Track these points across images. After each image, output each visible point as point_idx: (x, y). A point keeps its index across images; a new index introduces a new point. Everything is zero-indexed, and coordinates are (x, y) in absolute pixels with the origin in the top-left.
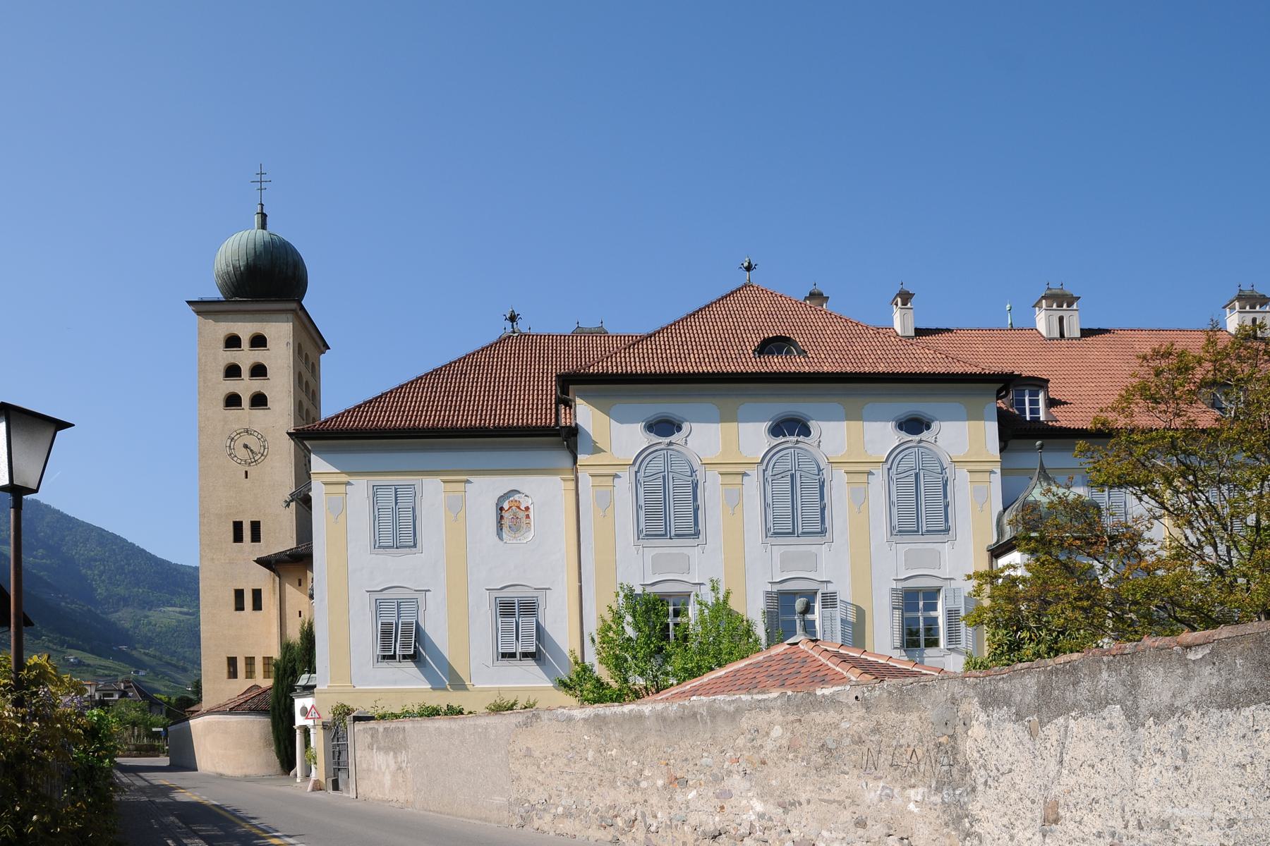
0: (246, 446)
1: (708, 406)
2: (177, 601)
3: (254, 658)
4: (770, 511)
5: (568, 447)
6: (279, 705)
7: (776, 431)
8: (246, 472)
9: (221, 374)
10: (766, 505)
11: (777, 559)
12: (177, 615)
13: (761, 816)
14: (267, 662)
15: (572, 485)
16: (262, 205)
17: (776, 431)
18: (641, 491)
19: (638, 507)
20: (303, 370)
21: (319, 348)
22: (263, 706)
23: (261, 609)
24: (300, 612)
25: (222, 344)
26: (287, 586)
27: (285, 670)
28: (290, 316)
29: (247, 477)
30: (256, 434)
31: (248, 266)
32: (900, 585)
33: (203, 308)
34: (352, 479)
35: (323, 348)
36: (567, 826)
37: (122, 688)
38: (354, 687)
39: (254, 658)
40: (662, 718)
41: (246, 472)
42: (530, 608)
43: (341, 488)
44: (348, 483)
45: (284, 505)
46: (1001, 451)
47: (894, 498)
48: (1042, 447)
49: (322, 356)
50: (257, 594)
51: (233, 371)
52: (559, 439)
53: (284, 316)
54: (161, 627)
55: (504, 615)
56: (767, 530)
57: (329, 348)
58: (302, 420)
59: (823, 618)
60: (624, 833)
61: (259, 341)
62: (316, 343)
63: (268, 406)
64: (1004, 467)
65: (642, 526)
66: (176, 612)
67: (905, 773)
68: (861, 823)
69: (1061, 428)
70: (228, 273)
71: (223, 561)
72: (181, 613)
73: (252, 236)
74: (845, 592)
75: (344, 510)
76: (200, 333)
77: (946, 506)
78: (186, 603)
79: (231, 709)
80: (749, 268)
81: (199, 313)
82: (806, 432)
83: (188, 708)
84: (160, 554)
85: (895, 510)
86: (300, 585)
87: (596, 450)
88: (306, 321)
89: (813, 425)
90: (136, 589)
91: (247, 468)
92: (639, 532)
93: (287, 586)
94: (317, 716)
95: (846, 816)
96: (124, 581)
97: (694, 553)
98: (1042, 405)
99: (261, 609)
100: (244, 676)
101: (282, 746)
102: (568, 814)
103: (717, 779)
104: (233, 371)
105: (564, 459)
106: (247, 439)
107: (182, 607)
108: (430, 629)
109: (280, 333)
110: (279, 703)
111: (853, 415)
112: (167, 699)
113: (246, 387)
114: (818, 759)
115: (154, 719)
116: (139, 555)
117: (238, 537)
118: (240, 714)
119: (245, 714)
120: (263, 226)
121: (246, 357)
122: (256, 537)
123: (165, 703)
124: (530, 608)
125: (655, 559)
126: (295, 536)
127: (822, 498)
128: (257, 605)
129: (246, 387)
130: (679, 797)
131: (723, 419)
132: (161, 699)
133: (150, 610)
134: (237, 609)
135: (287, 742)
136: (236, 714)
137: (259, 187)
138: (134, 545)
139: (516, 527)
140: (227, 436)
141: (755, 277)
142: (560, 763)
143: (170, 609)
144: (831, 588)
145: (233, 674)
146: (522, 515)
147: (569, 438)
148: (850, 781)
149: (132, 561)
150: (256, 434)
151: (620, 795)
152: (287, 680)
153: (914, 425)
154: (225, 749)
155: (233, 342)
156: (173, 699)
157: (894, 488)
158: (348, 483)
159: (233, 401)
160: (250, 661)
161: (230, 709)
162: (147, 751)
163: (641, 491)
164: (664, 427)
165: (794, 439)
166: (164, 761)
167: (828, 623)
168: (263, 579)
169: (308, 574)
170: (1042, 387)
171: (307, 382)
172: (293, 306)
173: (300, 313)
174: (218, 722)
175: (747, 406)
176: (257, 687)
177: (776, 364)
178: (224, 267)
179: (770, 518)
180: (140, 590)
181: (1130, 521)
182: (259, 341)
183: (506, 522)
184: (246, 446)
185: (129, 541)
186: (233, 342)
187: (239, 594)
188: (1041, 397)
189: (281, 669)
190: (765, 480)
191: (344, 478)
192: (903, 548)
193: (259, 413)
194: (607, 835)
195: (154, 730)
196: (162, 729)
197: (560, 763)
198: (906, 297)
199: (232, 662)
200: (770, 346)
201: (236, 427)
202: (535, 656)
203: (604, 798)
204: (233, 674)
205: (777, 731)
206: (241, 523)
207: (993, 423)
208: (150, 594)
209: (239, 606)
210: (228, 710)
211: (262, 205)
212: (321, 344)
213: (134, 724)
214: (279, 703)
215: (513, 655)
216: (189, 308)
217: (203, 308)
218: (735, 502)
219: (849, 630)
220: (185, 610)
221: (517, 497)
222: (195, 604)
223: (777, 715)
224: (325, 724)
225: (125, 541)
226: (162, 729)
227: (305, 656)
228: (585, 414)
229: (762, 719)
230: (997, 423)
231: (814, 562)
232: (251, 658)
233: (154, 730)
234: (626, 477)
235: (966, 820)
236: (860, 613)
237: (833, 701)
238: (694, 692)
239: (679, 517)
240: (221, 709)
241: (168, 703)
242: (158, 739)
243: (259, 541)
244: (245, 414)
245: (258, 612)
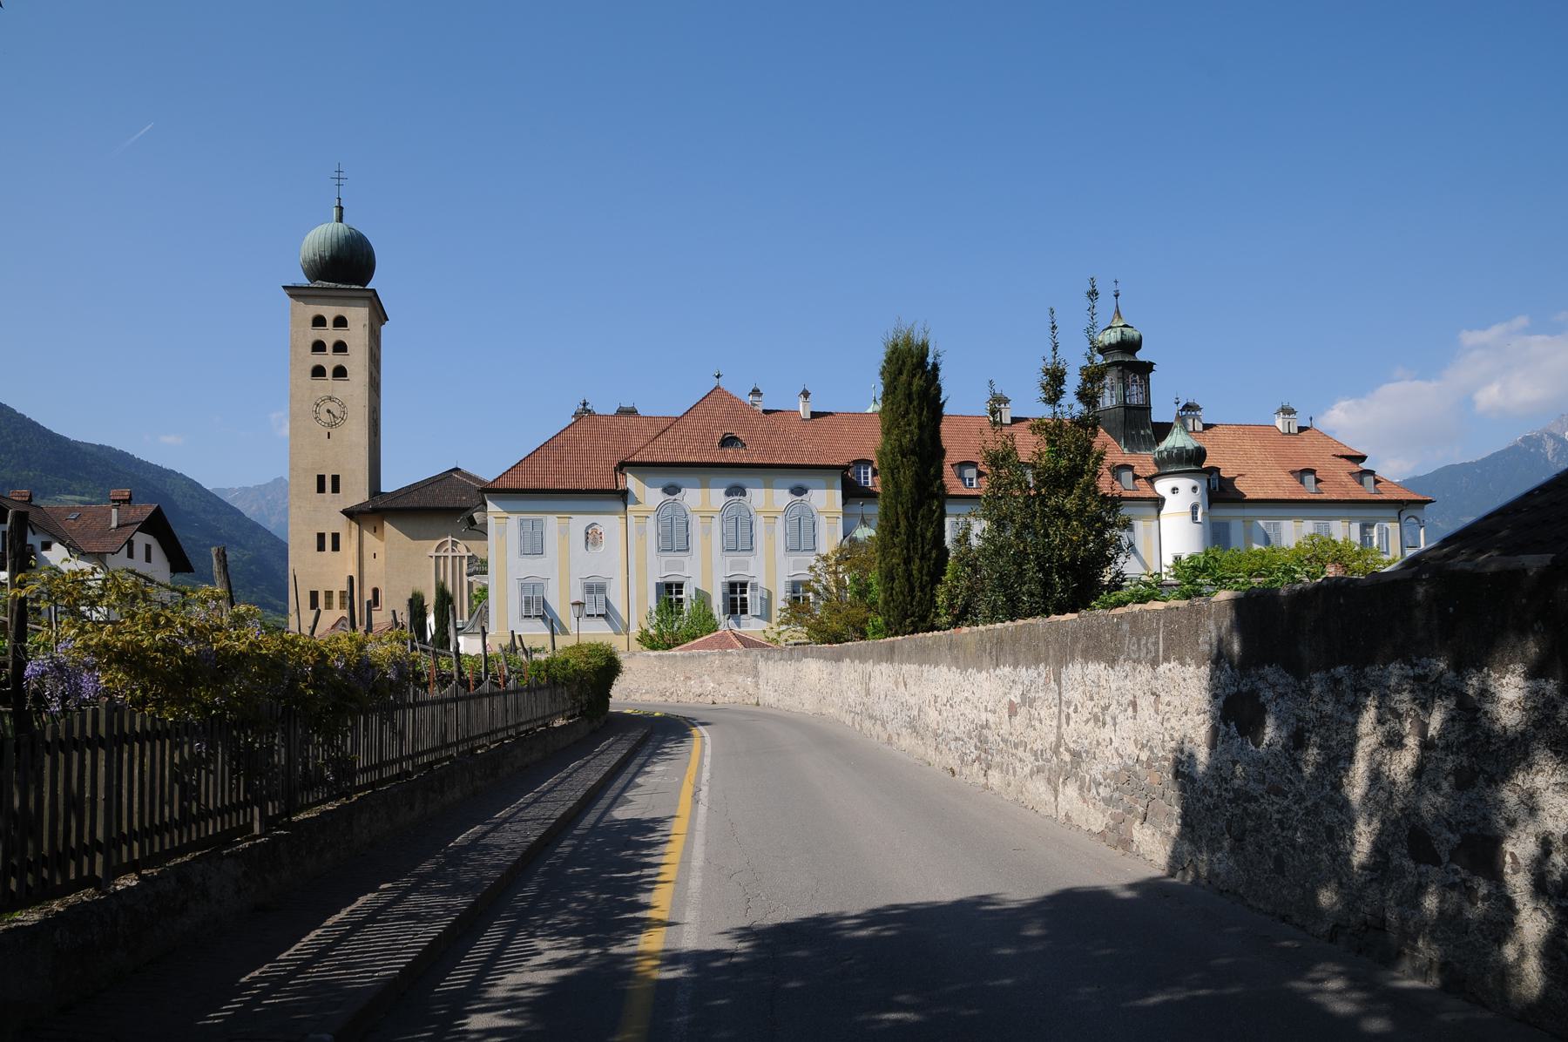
0: (329, 411)
1: (695, 479)
2: (75, 486)
4: (725, 538)
5: (623, 500)
7: (728, 494)
8: (329, 433)
9: (310, 349)
10: (723, 534)
11: (728, 565)
13: (713, 688)
15: (624, 520)
16: (339, 199)
17: (728, 494)
18: (660, 526)
19: (658, 534)
23: (338, 550)
26: (365, 532)
28: (367, 302)
29: (329, 437)
30: (337, 401)
31: (332, 257)
32: (791, 579)
33: (295, 292)
34: (510, 516)
36: (646, 697)
40: (683, 656)
41: (329, 433)
42: (601, 589)
44: (507, 518)
46: (843, 505)
47: (788, 531)
48: (862, 505)
50: (336, 537)
51: (318, 347)
52: (619, 495)
53: (361, 302)
55: (588, 592)
56: (723, 548)
59: (751, 596)
60: (669, 697)
61: (340, 322)
62: (380, 317)
63: (348, 377)
64: (846, 512)
65: (660, 545)
66: (76, 501)
67: (747, 674)
68: (738, 688)
70: (315, 261)
72: (81, 502)
73: (330, 229)
74: (762, 582)
76: (292, 313)
77: (814, 536)
78: (88, 490)
80: (718, 377)
81: (291, 296)
82: (744, 494)
84: (57, 429)
85: (788, 538)
86: (375, 531)
87: (637, 502)
89: (747, 490)
90: (26, 472)
91: (330, 430)
92: (659, 548)
93: (365, 532)
95: (734, 687)
96: (10, 462)
97: (686, 560)
98: (870, 475)
99: (338, 550)
102: (647, 692)
103: (700, 677)
104: (318, 347)
105: (619, 506)
106: (330, 405)
107: (82, 494)
108: (549, 601)
109: (358, 315)
111: (768, 486)
113: (329, 360)
114: (727, 670)
116: (31, 430)
120: (340, 219)
121: (330, 335)
124: (601, 589)
125: (666, 562)
126: (367, 488)
127: (751, 531)
129: (329, 360)
130: (688, 684)
131: (703, 486)
133: (42, 498)
134: (319, 550)
138: (24, 416)
139: (595, 544)
141: (722, 383)
142: (644, 673)
143: (69, 497)
144: (755, 580)
146: (598, 537)
147: (623, 496)
148: (735, 676)
149: (21, 437)
150: (337, 401)
151: (668, 684)
153: (799, 491)
155: (319, 321)
157: (788, 525)
158: (507, 518)
159: (318, 372)
160: (329, 594)
163: (660, 526)
164: (671, 490)
165: (737, 498)
167: (753, 599)
168: (341, 525)
169: (385, 529)
170: (869, 464)
173: (374, 299)
175: (714, 479)
177: (731, 455)
178: (311, 255)
179: (725, 541)
180: (31, 474)
181: (764, 625)
182: (340, 322)
183: (590, 541)
184: (329, 411)
185: (18, 412)
186: (319, 321)
187: (321, 537)
188: (870, 470)
190: (723, 520)
191: (506, 515)
192: (792, 559)
193: (340, 384)
194: (664, 698)
197: (644, 673)
198: (806, 394)
200: (728, 441)
201: (321, 395)
202: (605, 616)
203: (662, 685)
205: (717, 662)
207: (837, 491)
208: (44, 478)
209: (321, 547)
211: (339, 199)
212: (383, 317)
215: (593, 615)
216: (284, 293)
217: (295, 292)
218: (707, 532)
219: (764, 603)
220: (87, 498)
221: (595, 526)
222: (99, 492)
223: (717, 657)
225: (13, 411)
228: (632, 482)
229: (713, 658)
230: (840, 491)
231: (746, 565)
234: (653, 517)
235: (1455, 936)
236: (770, 593)
237: (731, 653)
238: (692, 647)
239: (678, 542)
243: (338, 492)
244: (328, 384)
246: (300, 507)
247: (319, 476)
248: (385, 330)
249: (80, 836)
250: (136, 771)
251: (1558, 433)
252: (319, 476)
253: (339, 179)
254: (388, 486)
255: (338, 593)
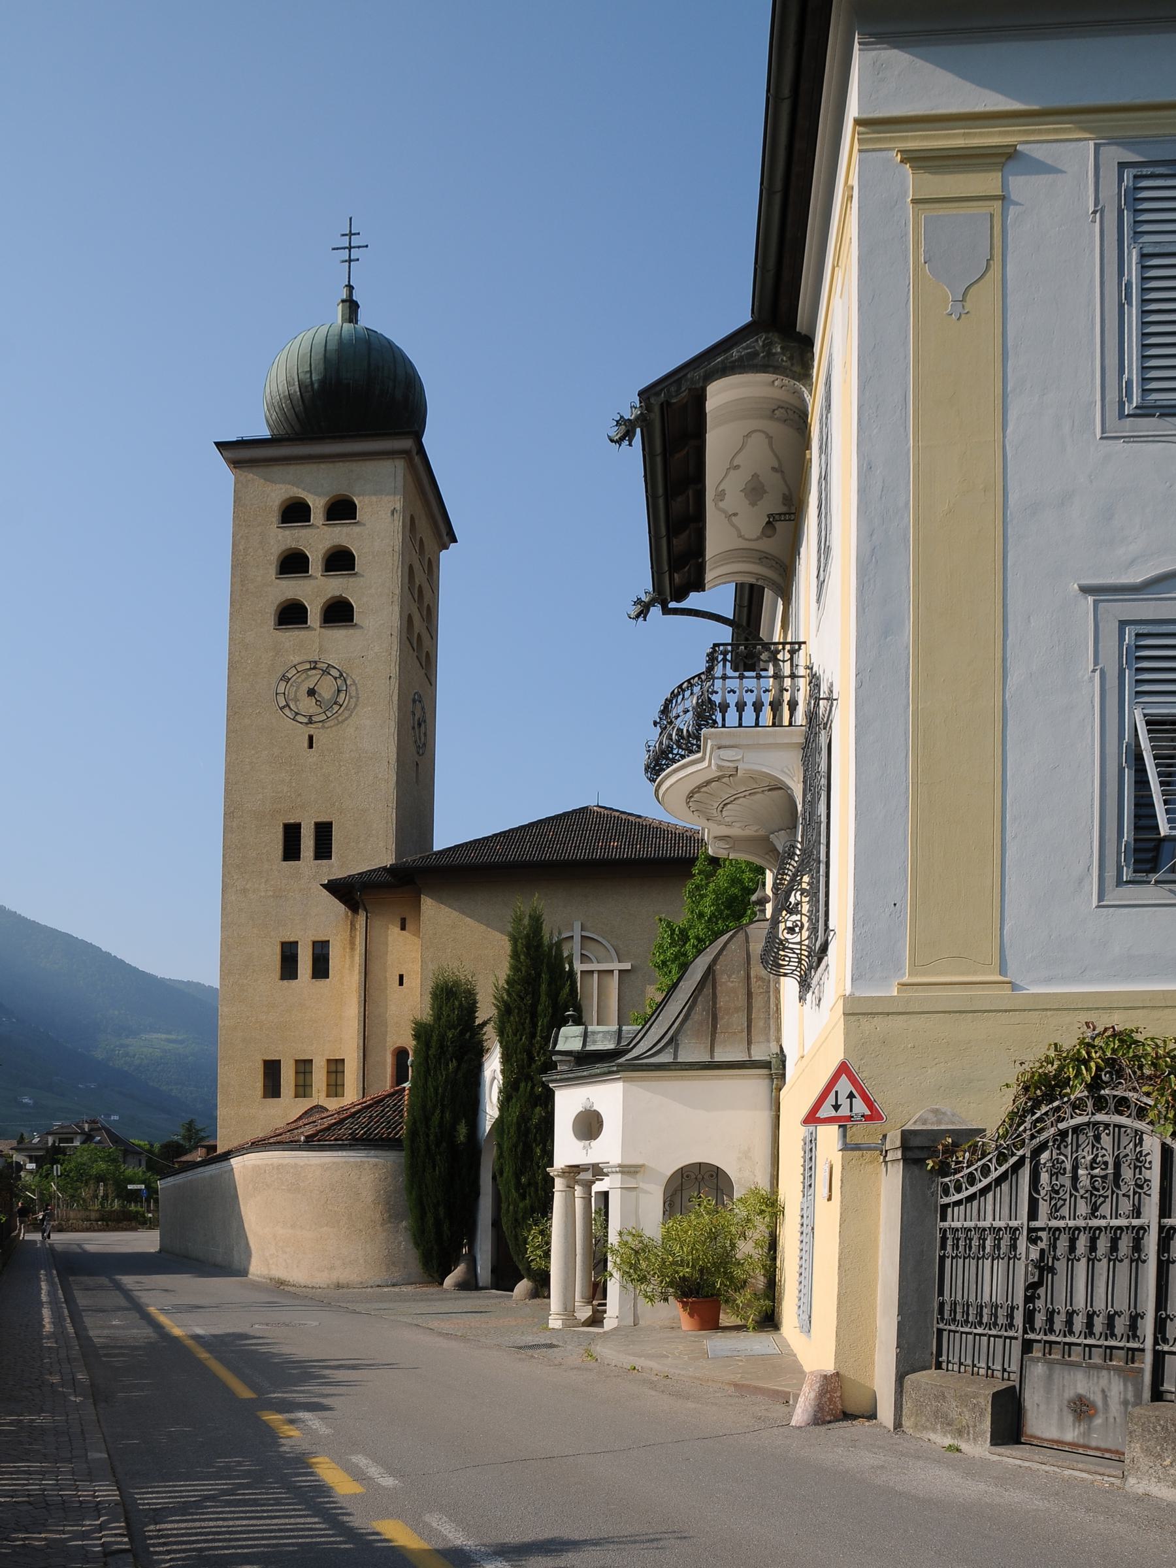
3: (311, 1061)
6: (428, 1127)
8: (311, 738)
9: (273, 570)
12: (162, 1043)
14: (333, 1068)
20: (417, 566)
21: (440, 536)
22: (381, 1131)
24: (401, 977)
25: (275, 517)
27: (442, 1046)
29: (311, 746)
31: (323, 382)
35: (446, 539)
37: (86, 1130)
38: (1014, 986)
39: (311, 1061)
41: (311, 738)
43: (986, 182)
45: (614, 432)
49: (443, 554)
54: (143, 1059)
57: (456, 541)
58: (411, 651)
69: (503, 1072)
71: (263, 894)
75: (996, 265)
79: (309, 1138)
83: (177, 1158)
88: (425, 481)
94: (860, 1107)
100: (292, 1093)
101: (430, 1220)
110: (427, 1120)
112: (148, 1146)
115: (129, 1172)
117: (291, 851)
118: (331, 1148)
119: (341, 1148)
122: (323, 850)
123: (146, 1151)
128: (321, 969)
132: (139, 1146)
135: (442, 1211)
136: (322, 1148)
137: (347, 258)
140: (280, 675)
145: (272, 1089)
152: (447, 1069)
154: (293, 1226)
155: (295, 512)
156: (157, 1146)
160: (304, 1067)
161: (307, 1137)
162: (119, 1221)
166: (146, 1241)
171: (420, 586)
172: (407, 444)
173: (417, 459)
174: (279, 1167)
176: (319, 1108)
178: (283, 387)
186: (295, 512)
189: (433, 1044)
193: (338, 635)
195: (130, 1187)
196: (143, 1187)
199: (272, 1070)
201: (296, 660)
204: (272, 1089)
206: (298, 826)
210: (302, 1138)
212: (444, 532)
213: (100, 1178)
214: (427, 1120)
220: (173, 1037)
224: (916, 1142)
226: (143, 1187)
227: (522, 999)
232: (305, 1061)
233: (130, 1187)
240: (286, 1137)
241: (150, 1151)
242: (136, 1202)
243: (330, 857)
245: (321, 983)
246: (244, 891)
247: (284, 945)
248: (448, 559)
249: (154, 1545)
250: (250, 1543)
251: (1085, 1394)
252: (284, 945)
253: (350, 248)
254: (443, 838)
255: (324, 1064)
